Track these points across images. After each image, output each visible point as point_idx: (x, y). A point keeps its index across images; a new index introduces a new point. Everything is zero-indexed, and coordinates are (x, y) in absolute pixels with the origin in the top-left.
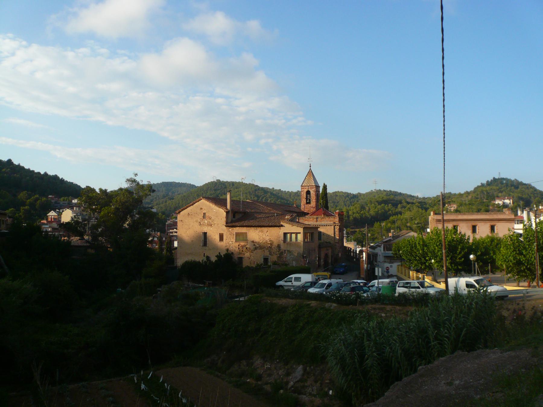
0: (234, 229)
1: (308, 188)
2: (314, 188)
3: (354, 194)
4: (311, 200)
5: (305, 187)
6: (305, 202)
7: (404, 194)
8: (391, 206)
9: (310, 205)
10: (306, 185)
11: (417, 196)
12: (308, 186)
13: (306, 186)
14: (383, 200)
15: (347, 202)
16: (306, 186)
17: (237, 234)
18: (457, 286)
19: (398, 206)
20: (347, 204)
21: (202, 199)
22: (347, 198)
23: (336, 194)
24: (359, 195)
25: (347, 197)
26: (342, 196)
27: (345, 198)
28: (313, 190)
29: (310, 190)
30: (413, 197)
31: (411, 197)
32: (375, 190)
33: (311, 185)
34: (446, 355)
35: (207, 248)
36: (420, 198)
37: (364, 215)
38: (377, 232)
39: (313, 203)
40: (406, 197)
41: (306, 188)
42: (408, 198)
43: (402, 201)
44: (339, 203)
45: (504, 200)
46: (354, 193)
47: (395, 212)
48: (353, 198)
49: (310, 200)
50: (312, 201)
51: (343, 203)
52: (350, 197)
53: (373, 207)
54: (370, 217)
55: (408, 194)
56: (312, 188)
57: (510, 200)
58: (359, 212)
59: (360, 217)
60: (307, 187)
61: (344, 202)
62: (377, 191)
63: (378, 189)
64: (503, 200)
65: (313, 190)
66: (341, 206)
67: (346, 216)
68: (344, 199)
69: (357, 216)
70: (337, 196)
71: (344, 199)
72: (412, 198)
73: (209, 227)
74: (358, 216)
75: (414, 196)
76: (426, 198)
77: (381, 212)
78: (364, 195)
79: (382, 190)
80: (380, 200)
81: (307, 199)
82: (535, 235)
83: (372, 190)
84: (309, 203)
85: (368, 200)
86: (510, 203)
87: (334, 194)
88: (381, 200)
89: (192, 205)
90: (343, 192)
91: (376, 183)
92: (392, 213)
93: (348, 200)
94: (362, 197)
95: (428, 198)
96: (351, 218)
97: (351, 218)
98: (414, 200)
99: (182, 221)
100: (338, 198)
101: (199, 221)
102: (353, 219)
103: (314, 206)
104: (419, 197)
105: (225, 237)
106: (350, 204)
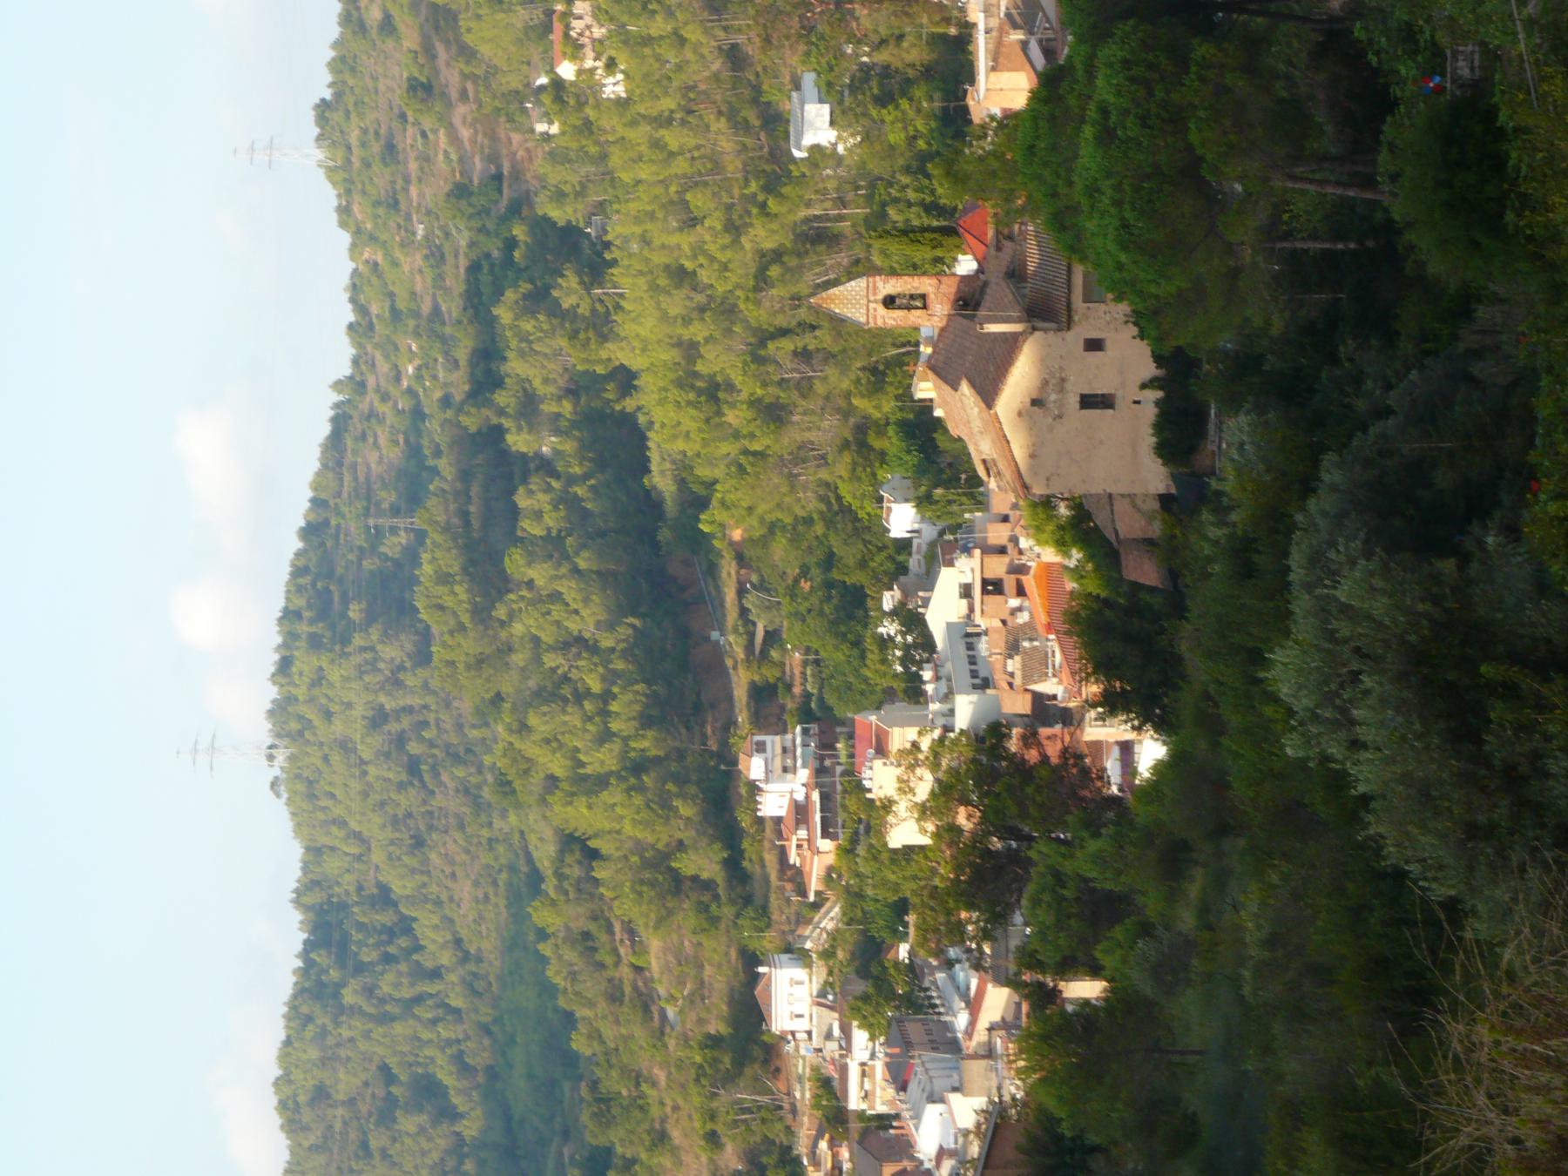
0: (1074, 306)
1: (876, 301)
2: (875, 283)
3: (306, 942)
4: (913, 292)
5: (871, 311)
6: (918, 313)
7: (317, 503)
9: (932, 296)
10: (863, 311)
11: (338, 385)
12: (869, 301)
13: (868, 310)
14: (465, 570)
15: (385, 988)
16: (868, 310)
17: (1088, 298)
19: (524, 449)
20: (407, 993)
21: (996, 414)
22: (349, 997)
23: (302, 1099)
24: (315, 898)
25: (337, 995)
26: (330, 1041)
27: (353, 1011)
28: (880, 284)
29: (880, 297)
30: (340, 423)
31: (349, 442)
32: (271, 758)
33: (864, 293)
35: (1119, 394)
36: (356, 362)
37: (620, 665)
38: (785, 489)
39: (925, 285)
40: (347, 478)
41: (875, 310)
42: (354, 466)
43: (473, 429)
44: (392, 1062)
46: (299, 947)
48: (344, 944)
49: (912, 297)
50: (917, 288)
51: (399, 1028)
52: (334, 974)
54: (631, 620)
55: (316, 465)
56: (875, 288)
59: (640, 687)
60: (872, 306)
61: (385, 1019)
62: (279, 736)
63: (262, 731)
66: (426, 1043)
67: (633, 781)
68: (350, 1029)
69: (625, 706)
70: (321, 1094)
71: (357, 1023)
72: (356, 425)
73: (1069, 386)
75: (335, 421)
76: (361, 309)
77: (585, 554)
78: (315, 852)
79: (272, 692)
80: (464, 597)
81: (909, 308)
83: (274, 785)
84: (923, 297)
85: (385, 767)
87: (307, 1116)
88: (468, 591)
89: (1008, 442)
90: (288, 1042)
91: (212, 748)
92: (586, 477)
93: (369, 991)
94: (332, 865)
95: (353, 300)
96: (647, 744)
97: (647, 744)
98: (371, 415)
99: (1048, 479)
100: (345, 1083)
101: (1050, 420)
102: (650, 733)
103: (934, 281)
104: (348, 371)
105: (1094, 335)
106: (403, 967)
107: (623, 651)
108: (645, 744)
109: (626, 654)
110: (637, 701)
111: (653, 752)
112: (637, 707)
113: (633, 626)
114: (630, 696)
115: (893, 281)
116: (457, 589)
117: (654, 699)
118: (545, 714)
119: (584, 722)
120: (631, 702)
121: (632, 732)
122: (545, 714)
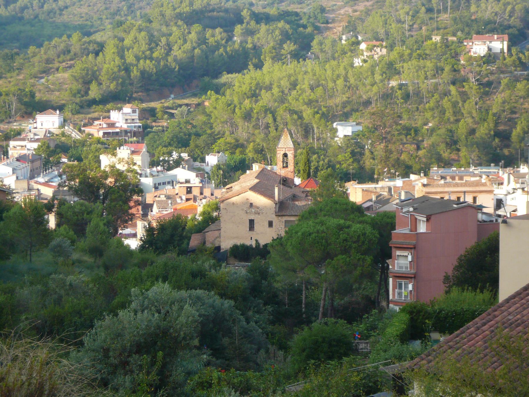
0: (283, 217)
8: (221, 33)
14: (194, 11)
18: (258, 243)
28: (291, 152)
29: (287, 152)
34: (516, 123)
35: (254, 233)
38: (222, 120)
39: (291, 167)
45: (491, 42)
47: (232, 51)
49: (287, 163)
53: (180, 39)
54: (177, 67)
57: (502, 42)
58: (148, 53)
60: (284, 149)
64: (488, 42)
65: (291, 152)
67: (122, 68)
69: (148, 65)
73: (257, 215)
74: (152, 67)
80: (185, 10)
81: (283, 162)
82: (426, 352)
84: (287, 167)
86: (502, 50)
96: (135, 73)
97: (135, 73)
102: (138, 74)
103: (292, 170)
105: (274, 224)
107: (167, 65)
108: (135, 72)
109: (166, 66)
110: (150, 69)
111: (132, 75)
112: (148, 69)
113: (175, 68)
114: (152, 67)
115: (292, 156)
116: (188, 8)
117: (150, 75)
118: (145, 37)
119: (142, 51)
120: (150, 67)
121: (139, 68)
122: (145, 37)
